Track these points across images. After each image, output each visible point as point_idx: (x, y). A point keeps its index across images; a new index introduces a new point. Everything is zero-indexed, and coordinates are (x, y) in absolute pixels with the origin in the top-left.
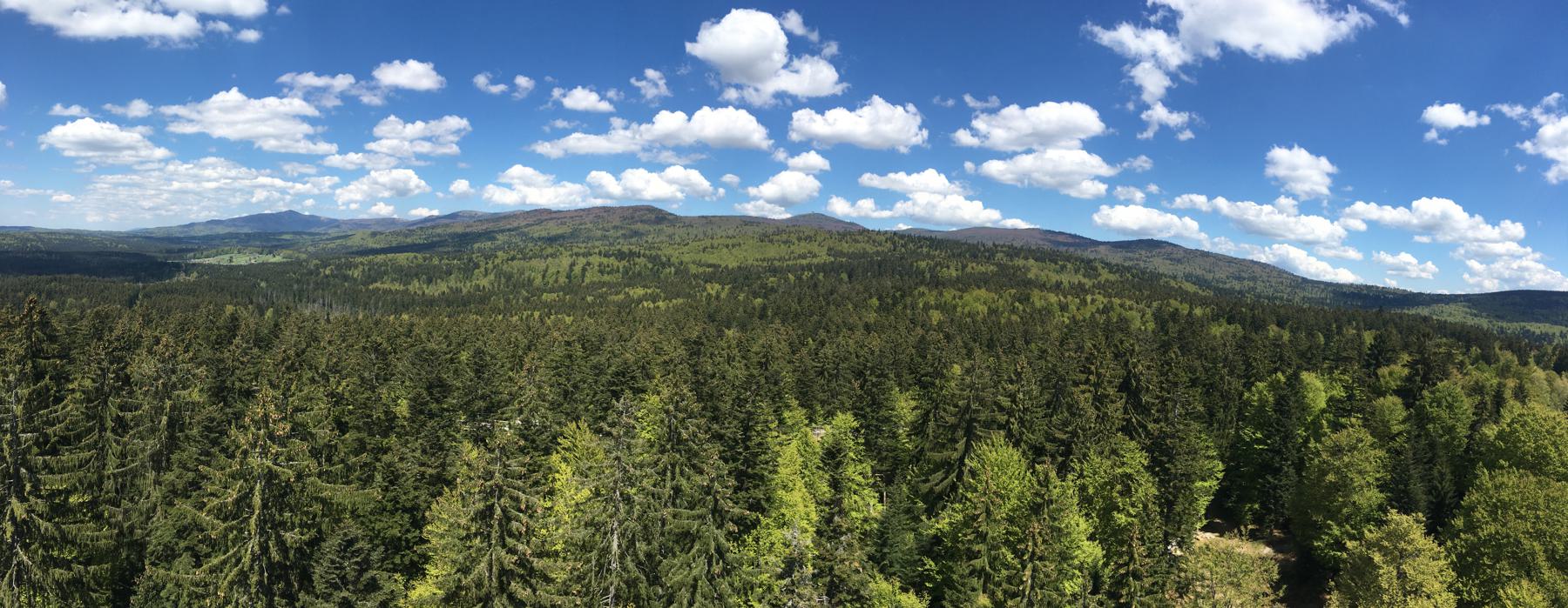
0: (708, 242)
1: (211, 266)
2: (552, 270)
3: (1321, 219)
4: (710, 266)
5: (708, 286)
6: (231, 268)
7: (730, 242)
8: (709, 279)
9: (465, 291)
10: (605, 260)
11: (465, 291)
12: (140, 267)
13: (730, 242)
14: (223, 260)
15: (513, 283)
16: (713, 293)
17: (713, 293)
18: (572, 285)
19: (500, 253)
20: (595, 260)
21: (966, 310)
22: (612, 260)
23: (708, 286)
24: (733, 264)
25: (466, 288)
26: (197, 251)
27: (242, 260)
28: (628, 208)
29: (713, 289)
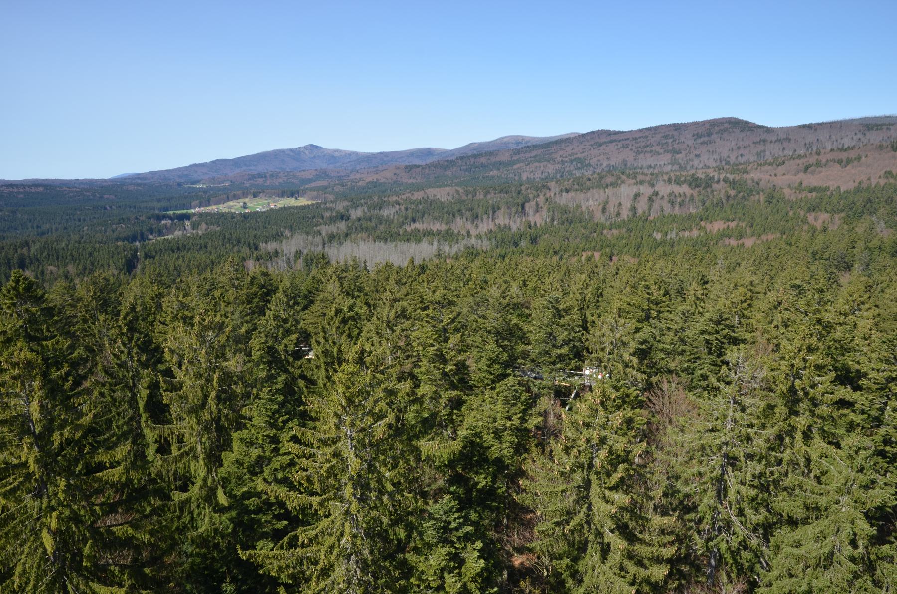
0: (812, 160)
1: (221, 215)
2: (613, 202)
3: (231, 158)
4: (812, 190)
5: (811, 218)
6: (245, 217)
7: (844, 156)
8: (813, 208)
9: (514, 228)
10: (677, 189)
11: (514, 228)
12: (130, 223)
13: (844, 156)
14: (235, 207)
15: (569, 218)
16: (818, 225)
17: (818, 225)
18: (637, 224)
19: (552, 185)
20: (664, 189)
21: (648, 476)
22: (685, 189)
23: (811, 218)
24: (847, 186)
25: (516, 225)
26: (206, 198)
27: (258, 205)
28: (704, 123)
29: (819, 219)
